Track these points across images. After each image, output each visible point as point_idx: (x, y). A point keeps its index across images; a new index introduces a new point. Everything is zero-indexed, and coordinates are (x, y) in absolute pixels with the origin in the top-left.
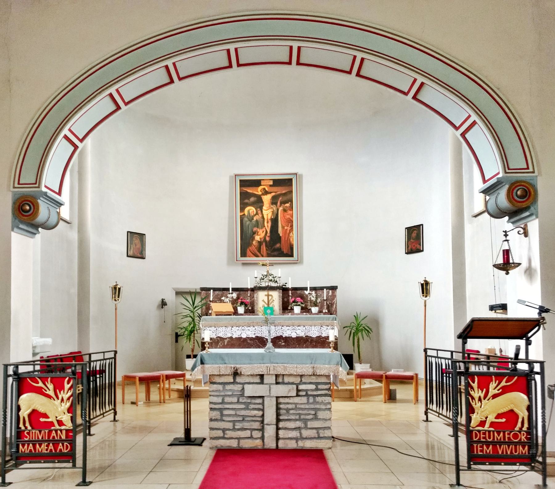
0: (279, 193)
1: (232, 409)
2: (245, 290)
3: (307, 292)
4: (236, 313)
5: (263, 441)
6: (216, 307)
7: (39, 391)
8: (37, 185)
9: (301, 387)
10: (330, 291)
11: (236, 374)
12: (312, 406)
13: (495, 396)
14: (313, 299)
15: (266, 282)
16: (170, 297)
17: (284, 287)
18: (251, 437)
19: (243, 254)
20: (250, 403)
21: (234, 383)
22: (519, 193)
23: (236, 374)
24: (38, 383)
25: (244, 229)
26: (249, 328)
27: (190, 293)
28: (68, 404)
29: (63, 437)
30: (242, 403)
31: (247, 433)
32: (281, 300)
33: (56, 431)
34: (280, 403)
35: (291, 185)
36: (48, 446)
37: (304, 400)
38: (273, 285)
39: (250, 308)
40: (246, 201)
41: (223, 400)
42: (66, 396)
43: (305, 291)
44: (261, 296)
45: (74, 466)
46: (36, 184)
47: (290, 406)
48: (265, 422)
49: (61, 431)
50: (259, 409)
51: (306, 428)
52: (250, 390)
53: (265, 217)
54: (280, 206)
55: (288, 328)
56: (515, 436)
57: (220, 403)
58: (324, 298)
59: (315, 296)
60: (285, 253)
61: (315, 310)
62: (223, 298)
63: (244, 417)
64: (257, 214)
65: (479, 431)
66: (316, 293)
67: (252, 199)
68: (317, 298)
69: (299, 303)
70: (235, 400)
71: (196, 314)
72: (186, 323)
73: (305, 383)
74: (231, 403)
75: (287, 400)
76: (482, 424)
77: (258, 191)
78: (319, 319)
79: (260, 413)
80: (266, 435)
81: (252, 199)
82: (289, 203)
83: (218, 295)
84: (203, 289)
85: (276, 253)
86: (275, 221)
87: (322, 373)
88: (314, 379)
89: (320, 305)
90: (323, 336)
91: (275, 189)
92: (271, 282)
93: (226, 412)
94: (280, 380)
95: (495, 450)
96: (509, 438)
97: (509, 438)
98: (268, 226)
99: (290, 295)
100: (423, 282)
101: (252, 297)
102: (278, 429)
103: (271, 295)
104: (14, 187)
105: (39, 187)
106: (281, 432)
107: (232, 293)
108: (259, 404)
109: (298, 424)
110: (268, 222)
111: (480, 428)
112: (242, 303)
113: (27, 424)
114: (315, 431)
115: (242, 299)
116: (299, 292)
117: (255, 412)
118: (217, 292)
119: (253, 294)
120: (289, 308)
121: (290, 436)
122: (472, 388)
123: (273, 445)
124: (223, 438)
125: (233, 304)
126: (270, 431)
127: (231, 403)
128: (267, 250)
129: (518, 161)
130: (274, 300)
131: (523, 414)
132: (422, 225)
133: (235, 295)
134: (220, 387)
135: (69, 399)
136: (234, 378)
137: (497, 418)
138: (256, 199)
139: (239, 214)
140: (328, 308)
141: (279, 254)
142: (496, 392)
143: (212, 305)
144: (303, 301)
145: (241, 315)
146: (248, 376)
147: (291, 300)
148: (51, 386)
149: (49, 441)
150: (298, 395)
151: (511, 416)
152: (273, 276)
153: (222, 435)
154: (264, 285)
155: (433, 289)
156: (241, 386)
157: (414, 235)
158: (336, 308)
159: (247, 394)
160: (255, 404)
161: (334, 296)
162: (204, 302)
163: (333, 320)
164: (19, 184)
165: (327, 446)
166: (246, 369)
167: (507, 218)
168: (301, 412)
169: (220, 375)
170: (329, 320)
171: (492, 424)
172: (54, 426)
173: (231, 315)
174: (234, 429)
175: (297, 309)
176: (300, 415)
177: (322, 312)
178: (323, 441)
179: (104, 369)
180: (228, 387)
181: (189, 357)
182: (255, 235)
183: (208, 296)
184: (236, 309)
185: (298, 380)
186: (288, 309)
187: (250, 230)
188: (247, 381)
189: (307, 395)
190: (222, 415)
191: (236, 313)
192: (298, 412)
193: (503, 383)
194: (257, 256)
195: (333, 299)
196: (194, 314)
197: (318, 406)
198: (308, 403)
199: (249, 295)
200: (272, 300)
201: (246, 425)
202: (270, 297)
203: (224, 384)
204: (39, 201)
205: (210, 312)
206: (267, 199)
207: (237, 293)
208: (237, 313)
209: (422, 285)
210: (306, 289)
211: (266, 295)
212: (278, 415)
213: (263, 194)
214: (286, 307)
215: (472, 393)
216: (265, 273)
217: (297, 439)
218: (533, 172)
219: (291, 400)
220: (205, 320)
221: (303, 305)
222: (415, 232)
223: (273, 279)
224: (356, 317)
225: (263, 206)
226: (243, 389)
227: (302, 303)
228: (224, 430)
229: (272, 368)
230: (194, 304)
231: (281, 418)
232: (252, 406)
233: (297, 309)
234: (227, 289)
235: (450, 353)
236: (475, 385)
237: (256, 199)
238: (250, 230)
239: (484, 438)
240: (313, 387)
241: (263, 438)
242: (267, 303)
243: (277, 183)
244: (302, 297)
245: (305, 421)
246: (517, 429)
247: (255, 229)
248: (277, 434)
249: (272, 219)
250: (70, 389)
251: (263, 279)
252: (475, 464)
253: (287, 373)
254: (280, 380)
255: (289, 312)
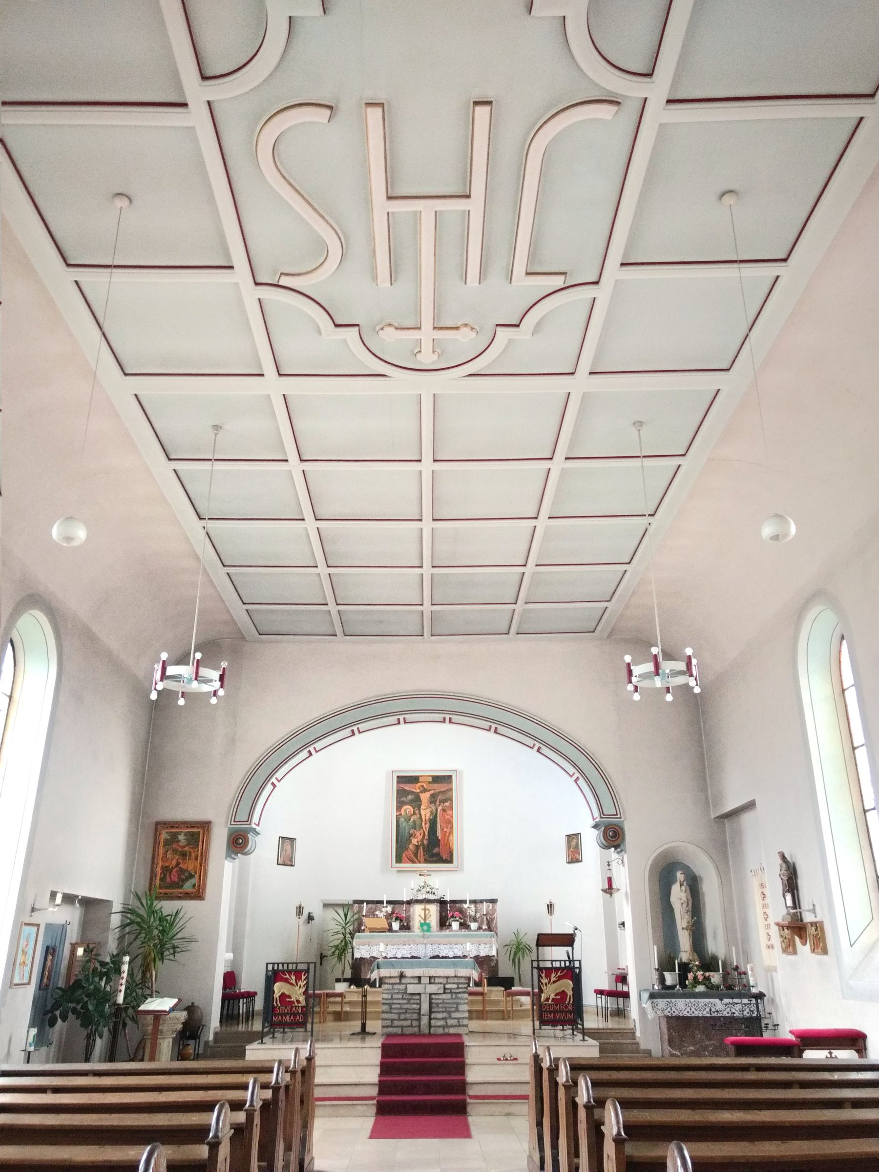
0: (438, 791)
1: (399, 1004)
2: (400, 903)
3: (465, 906)
4: (390, 930)
5: (420, 1028)
6: (368, 922)
7: (286, 981)
8: (249, 823)
9: (447, 986)
10: (491, 905)
11: (402, 976)
12: (454, 1001)
13: (554, 982)
14: (473, 914)
15: (423, 894)
16: (316, 909)
17: (442, 899)
18: (411, 1026)
19: (399, 860)
20: (411, 999)
21: (400, 983)
22: (611, 834)
23: (402, 976)
24: (286, 975)
25: (401, 831)
26: (404, 947)
27: (342, 906)
28: (304, 989)
29: (300, 1011)
30: (405, 999)
31: (408, 1023)
32: (439, 914)
33: (296, 1007)
34: (432, 999)
35: (451, 782)
36: (290, 1017)
37: (449, 996)
38: (432, 897)
39: (405, 924)
40: (403, 799)
41: (392, 996)
42: (302, 984)
43: (464, 905)
44: (417, 911)
45: (306, 1030)
46: (248, 821)
47: (439, 1001)
48: (422, 1013)
49: (299, 1007)
50: (417, 1004)
51: (450, 1018)
52: (411, 989)
53: (423, 817)
54: (439, 806)
55: (445, 946)
56: (566, 1007)
57: (390, 999)
58: (483, 912)
59: (474, 911)
60: (444, 858)
61: (474, 926)
62: (377, 913)
63: (407, 1009)
64: (414, 813)
65: (546, 1004)
66: (475, 907)
67: (410, 797)
68: (476, 912)
69: (457, 919)
70: (400, 996)
71: (348, 931)
72: (336, 940)
73: (450, 983)
74: (398, 999)
75: (437, 997)
76: (547, 999)
77: (416, 788)
78: (477, 936)
79: (417, 1007)
80: (422, 1023)
81: (410, 797)
82: (449, 802)
83: (371, 908)
84: (355, 902)
85: (434, 859)
86: (433, 823)
87: (461, 975)
88: (456, 980)
89: (480, 920)
90: (481, 956)
91: (435, 786)
92: (428, 894)
93: (394, 1006)
94: (432, 981)
95: (555, 1016)
96: (562, 1008)
97: (562, 1008)
98: (426, 827)
99: (449, 908)
100: (548, 903)
101: (407, 911)
102: (430, 1019)
103: (428, 910)
104: (231, 824)
105: (250, 824)
106: (433, 1022)
107: (386, 907)
108: (418, 999)
109: (445, 1015)
110: (426, 824)
111: (546, 1003)
112: (397, 918)
113: (278, 1003)
114: (456, 1021)
115: (397, 914)
116: (458, 905)
117: (415, 1006)
118: (370, 906)
119: (409, 908)
120: (447, 924)
121: (439, 1024)
122: (542, 978)
123: (426, 1031)
124: (391, 1026)
125: (387, 919)
126: (425, 1020)
127: (398, 999)
128: (424, 855)
129: (609, 809)
130: (431, 915)
131: (570, 993)
132: (580, 834)
133: (389, 909)
134: (390, 987)
135: (304, 986)
136: (400, 980)
137: (556, 995)
138: (413, 796)
139: (395, 814)
140: (489, 923)
141: (439, 860)
142: (555, 979)
143: (365, 920)
144: (462, 916)
145: (396, 931)
146: (410, 977)
147: (450, 914)
148: (293, 977)
149: (291, 1014)
150: (444, 993)
151: (563, 994)
152: (430, 887)
153: (390, 1024)
154: (421, 897)
155: (556, 909)
156: (405, 985)
157: (573, 843)
158: (496, 923)
159: (409, 991)
160: (414, 999)
161: (494, 910)
162: (356, 916)
163: (491, 937)
164: (234, 821)
165: (465, 1032)
166: (409, 972)
167: (613, 849)
168: (447, 1006)
169: (390, 977)
170: (487, 937)
171: (553, 1000)
172: (294, 1003)
173: (385, 932)
174: (399, 1020)
175: (455, 925)
176: (446, 1008)
177: (482, 928)
178: (462, 1028)
179: (227, 1002)
180: (396, 987)
181: (338, 980)
182: (412, 838)
183: (361, 910)
184: (390, 925)
185: (444, 981)
186: (446, 926)
187: (407, 831)
188: (409, 982)
189: (451, 993)
190: (391, 1008)
191: (390, 930)
192: (445, 1006)
193: (559, 974)
194: (414, 862)
195: (494, 914)
196: (345, 930)
197: (458, 1001)
198: (452, 998)
199: (404, 909)
200: (429, 915)
201: (408, 1016)
202: (427, 912)
203: (393, 984)
204: (249, 835)
205: (363, 928)
206: (425, 797)
207: (392, 906)
208: (392, 929)
209: (548, 905)
210: (465, 902)
211: (422, 909)
212: (431, 1007)
213: (421, 792)
214: (443, 923)
215: (542, 980)
216: (423, 884)
217: (443, 1027)
218: (621, 818)
219: (440, 997)
220: (359, 937)
221: (462, 921)
222: (574, 840)
223: (430, 891)
224: (517, 935)
225: (421, 804)
226: (406, 988)
227: (460, 918)
228: (392, 1020)
229: (427, 972)
230: (346, 918)
231: (433, 1010)
232: (412, 1001)
233: (455, 925)
234: (381, 902)
235: (559, 962)
236: (543, 975)
237: (413, 796)
238: (407, 831)
239: (549, 1009)
240: (455, 986)
241: (419, 1026)
242: (423, 917)
243: (437, 779)
244: (462, 912)
245: (450, 1013)
246: (567, 1002)
247: (412, 831)
248: (430, 1023)
249: (430, 820)
250: (305, 979)
251: (420, 891)
252: (543, 1025)
253: (437, 975)
254: (432, 981)
255: (448, 929)
